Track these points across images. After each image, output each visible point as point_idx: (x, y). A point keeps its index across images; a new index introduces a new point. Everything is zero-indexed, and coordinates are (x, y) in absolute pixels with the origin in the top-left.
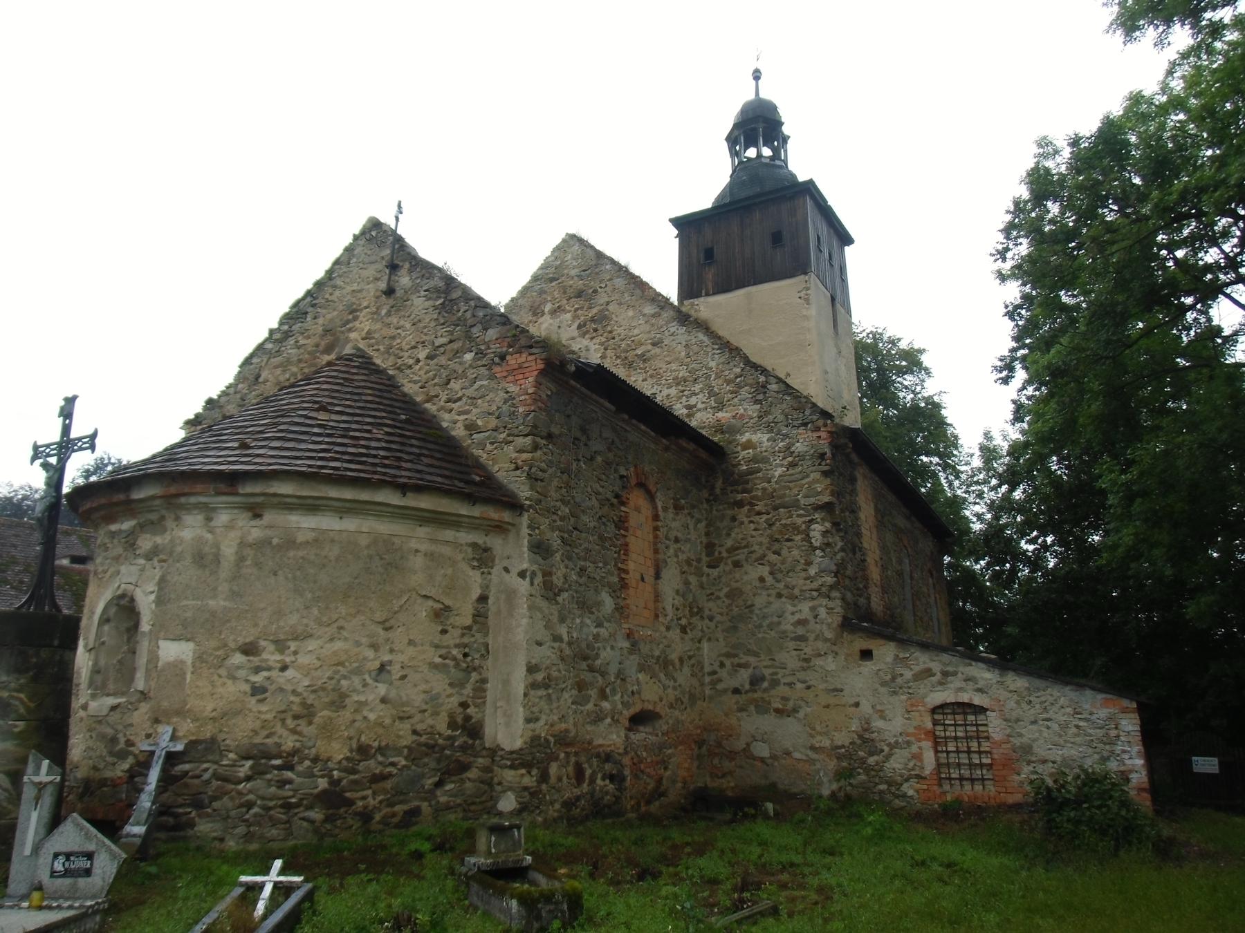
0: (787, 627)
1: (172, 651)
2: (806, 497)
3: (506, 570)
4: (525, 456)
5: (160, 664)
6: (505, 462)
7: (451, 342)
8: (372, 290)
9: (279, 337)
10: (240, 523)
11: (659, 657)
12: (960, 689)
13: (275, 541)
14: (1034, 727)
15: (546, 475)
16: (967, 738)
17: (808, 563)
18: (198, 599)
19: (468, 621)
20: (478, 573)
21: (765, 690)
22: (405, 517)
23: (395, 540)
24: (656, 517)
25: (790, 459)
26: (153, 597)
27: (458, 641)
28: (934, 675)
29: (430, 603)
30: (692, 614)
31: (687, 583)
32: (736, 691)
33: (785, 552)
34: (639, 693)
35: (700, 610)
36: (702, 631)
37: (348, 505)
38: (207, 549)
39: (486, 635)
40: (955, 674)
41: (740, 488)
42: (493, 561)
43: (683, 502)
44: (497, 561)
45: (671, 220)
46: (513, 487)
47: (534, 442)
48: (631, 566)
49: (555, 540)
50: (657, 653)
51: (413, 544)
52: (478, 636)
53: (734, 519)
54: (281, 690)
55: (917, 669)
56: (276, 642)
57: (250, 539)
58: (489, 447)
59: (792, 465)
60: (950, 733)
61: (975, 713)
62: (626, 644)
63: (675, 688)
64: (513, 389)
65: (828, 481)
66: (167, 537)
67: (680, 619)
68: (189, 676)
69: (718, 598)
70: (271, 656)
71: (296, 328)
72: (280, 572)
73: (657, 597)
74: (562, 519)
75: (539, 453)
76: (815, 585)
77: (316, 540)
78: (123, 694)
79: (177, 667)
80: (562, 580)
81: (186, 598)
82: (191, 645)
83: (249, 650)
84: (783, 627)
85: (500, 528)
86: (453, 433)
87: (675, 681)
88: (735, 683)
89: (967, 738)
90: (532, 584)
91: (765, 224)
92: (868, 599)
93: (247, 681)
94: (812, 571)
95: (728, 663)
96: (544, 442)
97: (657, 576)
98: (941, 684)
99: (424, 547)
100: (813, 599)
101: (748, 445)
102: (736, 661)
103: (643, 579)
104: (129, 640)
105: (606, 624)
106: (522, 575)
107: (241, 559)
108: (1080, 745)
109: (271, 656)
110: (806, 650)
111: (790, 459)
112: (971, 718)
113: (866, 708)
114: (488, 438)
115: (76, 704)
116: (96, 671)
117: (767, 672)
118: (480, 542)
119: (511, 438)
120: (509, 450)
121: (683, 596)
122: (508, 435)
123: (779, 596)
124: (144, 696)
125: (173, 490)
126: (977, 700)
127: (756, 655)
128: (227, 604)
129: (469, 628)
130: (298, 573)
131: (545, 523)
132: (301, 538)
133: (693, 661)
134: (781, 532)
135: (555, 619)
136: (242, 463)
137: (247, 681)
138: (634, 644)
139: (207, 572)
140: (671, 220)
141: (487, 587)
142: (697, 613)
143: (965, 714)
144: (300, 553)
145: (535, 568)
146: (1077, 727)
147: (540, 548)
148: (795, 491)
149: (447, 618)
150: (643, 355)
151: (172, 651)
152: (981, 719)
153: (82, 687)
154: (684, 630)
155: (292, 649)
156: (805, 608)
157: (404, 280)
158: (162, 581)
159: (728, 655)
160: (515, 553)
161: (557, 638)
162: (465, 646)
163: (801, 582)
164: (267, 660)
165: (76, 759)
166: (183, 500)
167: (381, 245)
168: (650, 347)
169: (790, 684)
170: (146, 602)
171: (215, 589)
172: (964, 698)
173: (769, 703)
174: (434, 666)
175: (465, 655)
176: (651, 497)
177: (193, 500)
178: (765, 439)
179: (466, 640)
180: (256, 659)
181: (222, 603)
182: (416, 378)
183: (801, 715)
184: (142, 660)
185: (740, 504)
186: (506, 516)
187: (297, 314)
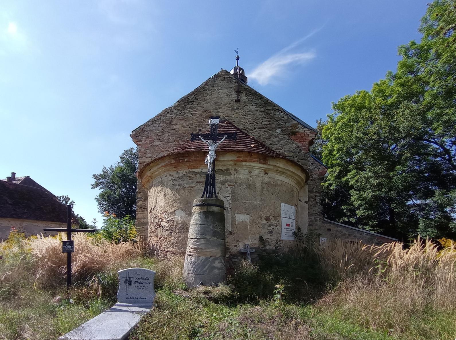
1: (240, 218)
7: (270, 124)
26: (229, 198)
38: (251, 183)
55: (342, 233)
66: (232, 177)
68: (248, 227)
70: (273, 222)
79: (244, 223)
81: (245, 200)
83: (268, 219)
93: (268, 229)
94: (316, 208)
98: (347, 237)
100: (315, 215)
106: (306, 202)
107: (263, 188)
109: (273, 222)
139: (252, 192)
148: (312, 187)
151: (240, 218)
155: (278, 220)
158: (232, 193)
163: (312, 211)
164: (272, 223)
166: (244, 163)
171: (255, 197)
182: (255, 134)
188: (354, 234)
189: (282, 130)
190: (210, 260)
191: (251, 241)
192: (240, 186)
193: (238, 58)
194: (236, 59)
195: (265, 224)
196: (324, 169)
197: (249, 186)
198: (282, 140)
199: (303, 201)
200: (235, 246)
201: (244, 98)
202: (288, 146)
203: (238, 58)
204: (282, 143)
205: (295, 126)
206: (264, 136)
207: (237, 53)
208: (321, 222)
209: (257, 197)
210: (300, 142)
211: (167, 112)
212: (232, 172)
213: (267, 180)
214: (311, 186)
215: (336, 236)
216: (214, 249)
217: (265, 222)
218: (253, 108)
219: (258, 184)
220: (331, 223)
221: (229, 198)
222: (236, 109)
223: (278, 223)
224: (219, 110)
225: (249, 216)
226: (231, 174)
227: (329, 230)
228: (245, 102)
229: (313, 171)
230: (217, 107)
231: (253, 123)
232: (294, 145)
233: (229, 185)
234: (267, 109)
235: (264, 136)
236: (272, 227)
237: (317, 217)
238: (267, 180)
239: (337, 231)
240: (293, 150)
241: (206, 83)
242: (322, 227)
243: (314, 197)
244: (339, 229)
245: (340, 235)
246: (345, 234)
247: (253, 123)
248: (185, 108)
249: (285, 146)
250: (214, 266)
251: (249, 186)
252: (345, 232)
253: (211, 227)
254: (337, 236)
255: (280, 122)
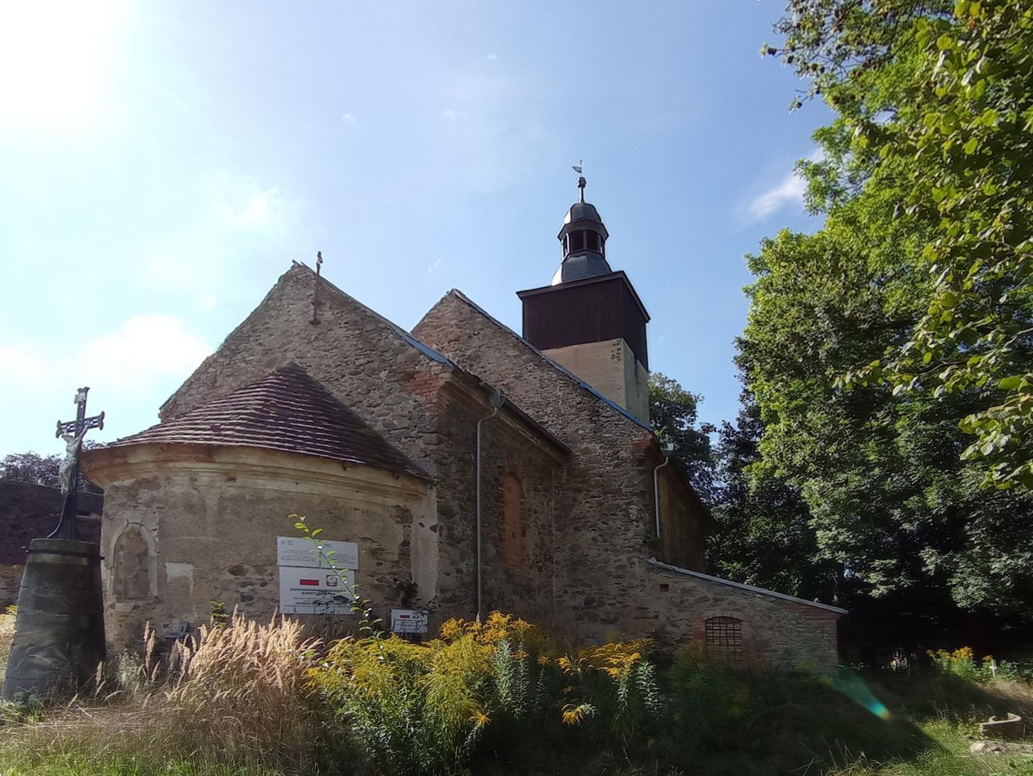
0: (611, 569)
1: (176, 570)
2: (626, 487)
3: (421, 525)
4: (432, 447)
5: (168, 579)
6: (415, 449)
7: (368, 362)
8: (300, 322)
9: (129, 438)
10: (219, 484)
11: (525, 586)
12: (725, 609)
13: (248, 497)
14: (771, 632)
15: (448, 461)
16: (727, 637)
17: (627, 530)
18: (192, 535)
19: (396, 558)
20: (401, 526)
21: (595, 608)
22: (347, 485)
23: (339, 500)
24: (522, 496)
25: (616, 461)
26: (155, 533)
27: (389, 570)
28: (709, 600)
29: (368, 544)
30: (546, 560)
31: (542, 540)
32: (575, 608)
33: (611, 523)
34: (513, 607)
35: (551, 557)
36: (552, 570)
37: (302, 474)
39: (409, 567)
40: (722, 600)
41: (579, 480)
42: (412, 518)
43: (540, 487)
44: (414, 519)
45: (517, 293)
46: (426, 469)
47: (439, 437)
48: (506, 527)
49: (455, 506)
50: (523, 584)
51: (353, 504)
52: (404, 568)
53: (575, 500)
54: (263, 598)
55: (697, 596)
56: (256, 566)
57: (228, 495)
58: (403, 440)
59: (617, 465)
60: (717, 634)
61: (733, 623)
62: (504, 577)
63: (535, 605)
64: (421, 399)
65: (643, 477)
66: (162, 492)
67: (538, 562)
68: (192, 588)
69: (564, 550)
71: (242, 347)
72: (254, 519)
73: (524, 548)
74: (460, 492)
75: (442, 445)
76: (631, 544)
77: (280, 498)
78: (141, 599)
79: (182, 581)
80: (461, 533)
82: (191, 567)
83: (236, 571)
84: (609, 570)
85: (416, 497)
86: (376, 429)
87: (535, 601)
88: (576, 604)
89: (727, 637)
90: (441, 535)
91: (592, 301)
92: (663, 554)
93: (237, 592)
94: (630, 534)
95: (570, 590)
96: (446, 438)
97: (524, 534)
98: (712, 606)
99: (362, 506)
100: (629, 552)
101: (587, 451)
102: (576, 589)
103: (514, 537)
104: (140, 562)
105: (491, 564)
106: (433, 528)
107: (222, 509)
108: (799, 642)
109: (252, 575)
110: (624, 584)
111: (616, 461)
112: (730, 626)
113: (662, 619)
114: (403, 433)
115: (106, 604)
116: (117, 581)
117: (596, 597)
118: (402, 505)
119: (421, 434)
120: (421, 443)
121: (540, 548)
122: (418, 432)
123: (606, 550)
124: (158, 600)
125: (161, 457)
126: (736, 615)
127: (589, 586)
128: (216, 540)
129: (397, 562)
130: (268, 520)
131: (449, 494)
132: (267, 496)
133: (546, 589)
134: (608, 510)
135: (457, 558)
136: (216, 440)
137: (237, 592)
138: (510, 577)
139: (197, 517)
140: (517, 293)
141: (408, 535)
142: (549, 559)
143: (727, 623)
144: (269, 507)
145: (442, 524)
146: (799, 632)
147: (444, 512)
148: (619, 483)
149: (382, 554)
150: (508, 384)
151: (176, 570)
152: (737, 626)
153: (108, 593)
154: (540, 569)
155: (269, 571)
156: (624, 558)
157: (328, 315)
159: (570, 586)
160: (427, 512)
161: (459, 571)
162: (395, 574)
165: (111, 640)
166: (171, 465)
167: (306, 286)
168: (512, 380)
169: (612, 605)
170: (151, 538)
171: (205, 529)
172: (727, 614)
173: (598, 615)
174: (376, 587)
175: (395, 580)
176: (519, 482)
177: (179, 465)
178: (598, 448)
179: (395, 570)
180: (242, 577)
181: (211, 539)
182: (343, 388)
183: (619, 622)
184: (153, 576)
185: (579, 490)
186: (421, 488)
187: (236, 342)
188: (731, 598)
189: (390, 372)
190: (26, 651)
191: (196, 615)
192: (174, 508)
193: (582, 183)
194: (579, 186)
195: (230, 582)
196: (645, 436)
197: (190, 508)
198: (389, 392)
199: (427, 527)
200: (166, 626)
201: (328, 315)
202: (401, 405)
203: (582, 183)
204: (388, 400)
205: (414, 360)
206: (359, 390)
207: (580, 172)
208: (643, 569)
209: (208, 529)
210: (421, 394)
211: (209, 363)
212: (162, 482)
213: (232, 493)
214: (616, 479)
215: (682, 602)
216: (35, 632)
217: (230, 577)
218: (340, 332)
219: (212, 502)
220: (668, 570)
221: (155, 533)
222: (315, 340)
223: (266, 578)
224: (287, 347)
225: (192, 566)
226: (160, 487)
227: (665, 587)
228: (329, 323)
229: (619, 441)
230: (285, 341)
231: (340, 365)
232: (411, 402)
233: (157, 508)
234: (366, 332)
235: (359, 390)
236: (250, 587)
237: (634, 557)
238: (231, 491)
239: (684, 591)
240: (410, 412)
241: (270, 297)
242: (646, 582)
243: (624, 506)
244: (690, 584)
245: (692, 599)
246: (705, 599)
247: (340, 365)
248: (235, 352)
249: (394, 407)
250: (32, 663)
251: (190, 508)
252: (707, 594)
253: (33, 592)
254: (686, 602)
255: (387, 354)
